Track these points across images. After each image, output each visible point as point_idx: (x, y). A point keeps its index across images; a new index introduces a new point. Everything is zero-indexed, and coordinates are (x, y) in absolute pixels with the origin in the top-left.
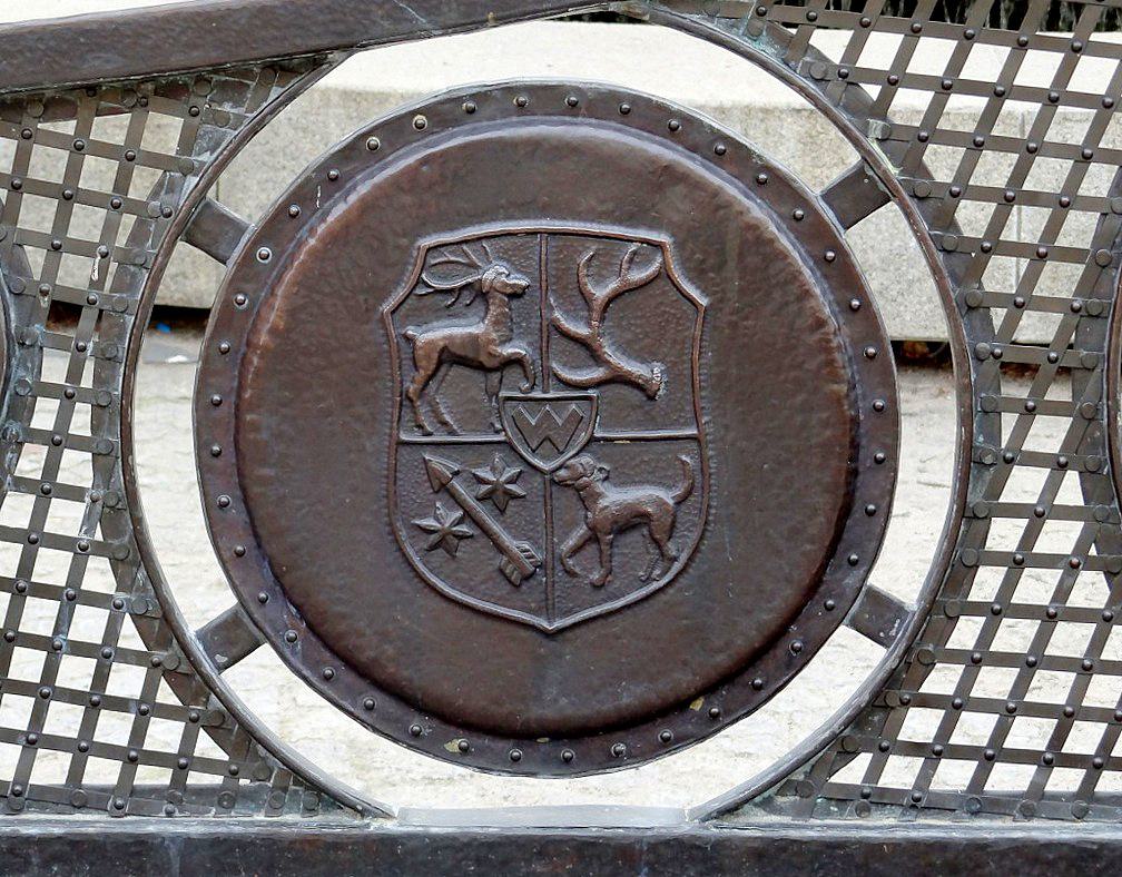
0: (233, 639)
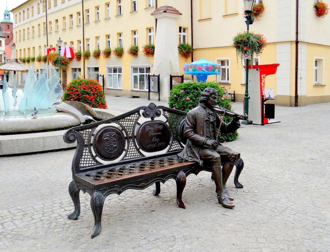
0: (96, 156)
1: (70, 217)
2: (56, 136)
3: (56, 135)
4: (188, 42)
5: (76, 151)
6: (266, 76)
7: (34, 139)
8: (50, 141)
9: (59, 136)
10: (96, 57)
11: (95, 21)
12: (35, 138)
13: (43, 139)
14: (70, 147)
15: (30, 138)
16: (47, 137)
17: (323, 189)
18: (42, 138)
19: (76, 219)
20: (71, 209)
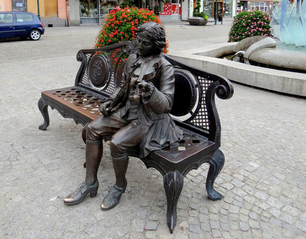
1: (41, 128)
2: (269, 75)
3: (269, 74)
4: (208, 24)
5: (170, 87)
6: (151, 60)
7: (248, 72)
8: (262, 78)
9: (272, 75)
10: (98, 25)
11: (88, 8)
12: (249, 71)
13: (256, 74)
14: (284, 92)
15: (245, 70)
16: (259, 73)
17: (279, 227)
18: (255, 73)
19: (45, 130)
20: (41, 120)
